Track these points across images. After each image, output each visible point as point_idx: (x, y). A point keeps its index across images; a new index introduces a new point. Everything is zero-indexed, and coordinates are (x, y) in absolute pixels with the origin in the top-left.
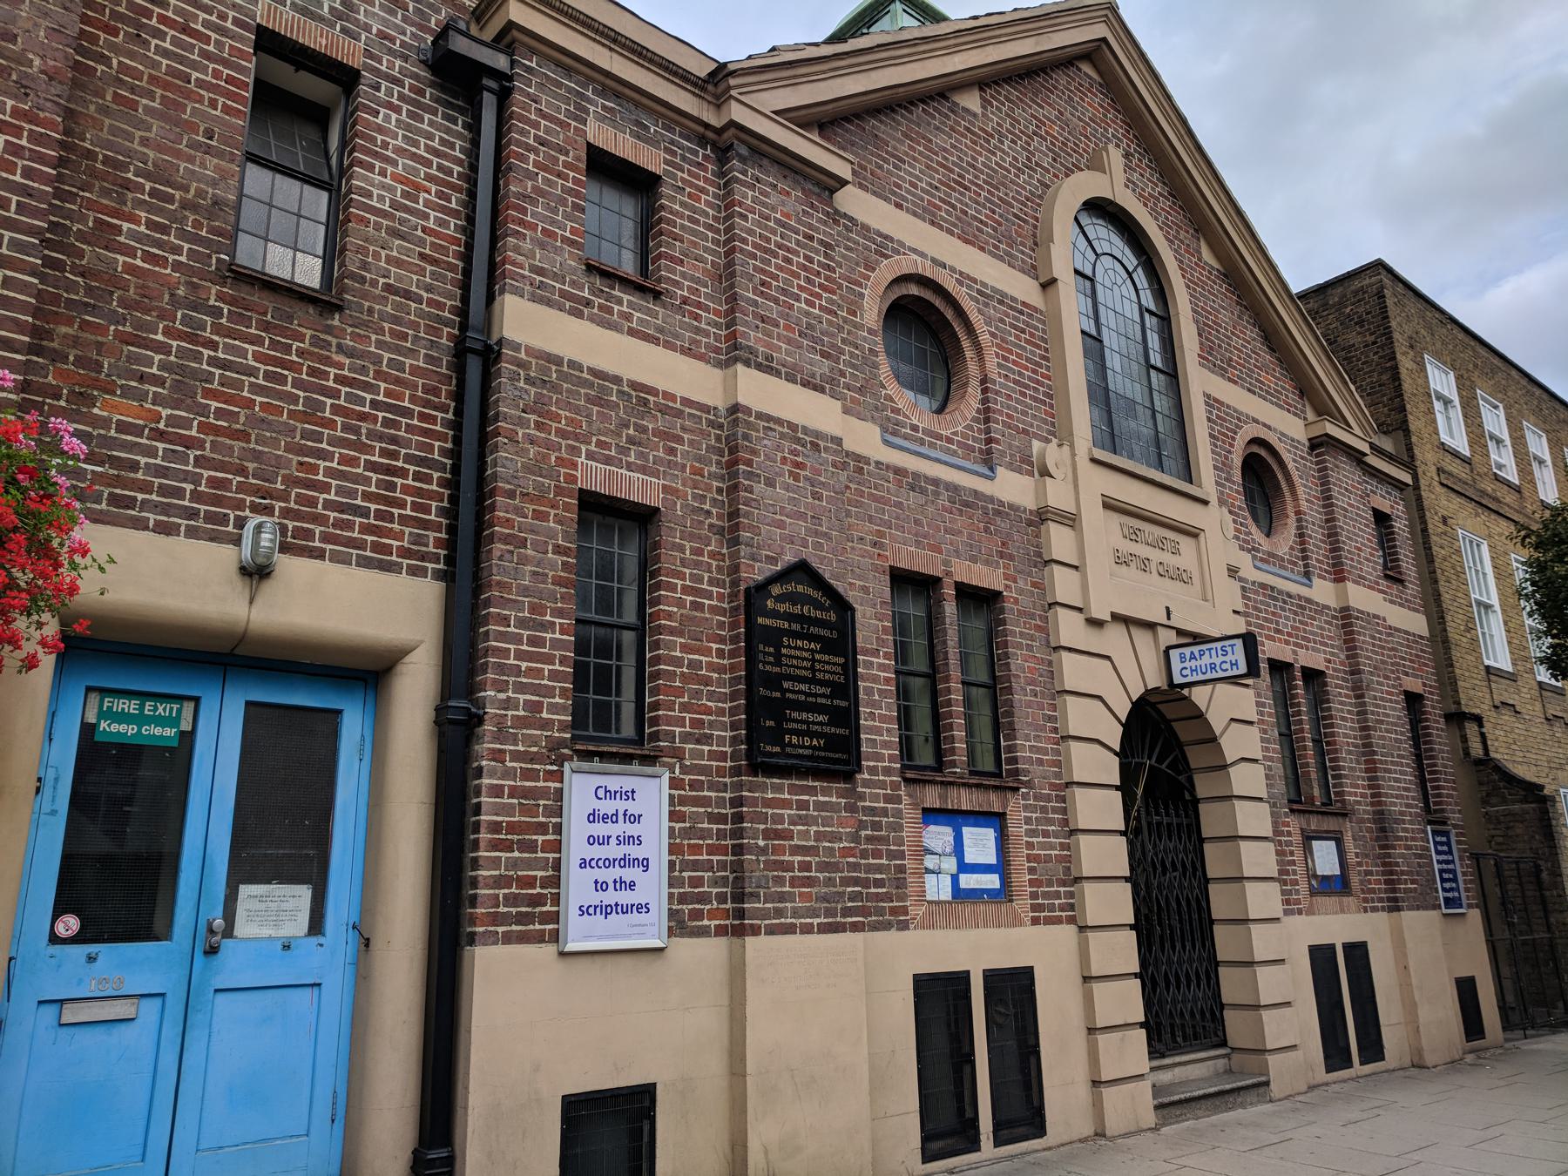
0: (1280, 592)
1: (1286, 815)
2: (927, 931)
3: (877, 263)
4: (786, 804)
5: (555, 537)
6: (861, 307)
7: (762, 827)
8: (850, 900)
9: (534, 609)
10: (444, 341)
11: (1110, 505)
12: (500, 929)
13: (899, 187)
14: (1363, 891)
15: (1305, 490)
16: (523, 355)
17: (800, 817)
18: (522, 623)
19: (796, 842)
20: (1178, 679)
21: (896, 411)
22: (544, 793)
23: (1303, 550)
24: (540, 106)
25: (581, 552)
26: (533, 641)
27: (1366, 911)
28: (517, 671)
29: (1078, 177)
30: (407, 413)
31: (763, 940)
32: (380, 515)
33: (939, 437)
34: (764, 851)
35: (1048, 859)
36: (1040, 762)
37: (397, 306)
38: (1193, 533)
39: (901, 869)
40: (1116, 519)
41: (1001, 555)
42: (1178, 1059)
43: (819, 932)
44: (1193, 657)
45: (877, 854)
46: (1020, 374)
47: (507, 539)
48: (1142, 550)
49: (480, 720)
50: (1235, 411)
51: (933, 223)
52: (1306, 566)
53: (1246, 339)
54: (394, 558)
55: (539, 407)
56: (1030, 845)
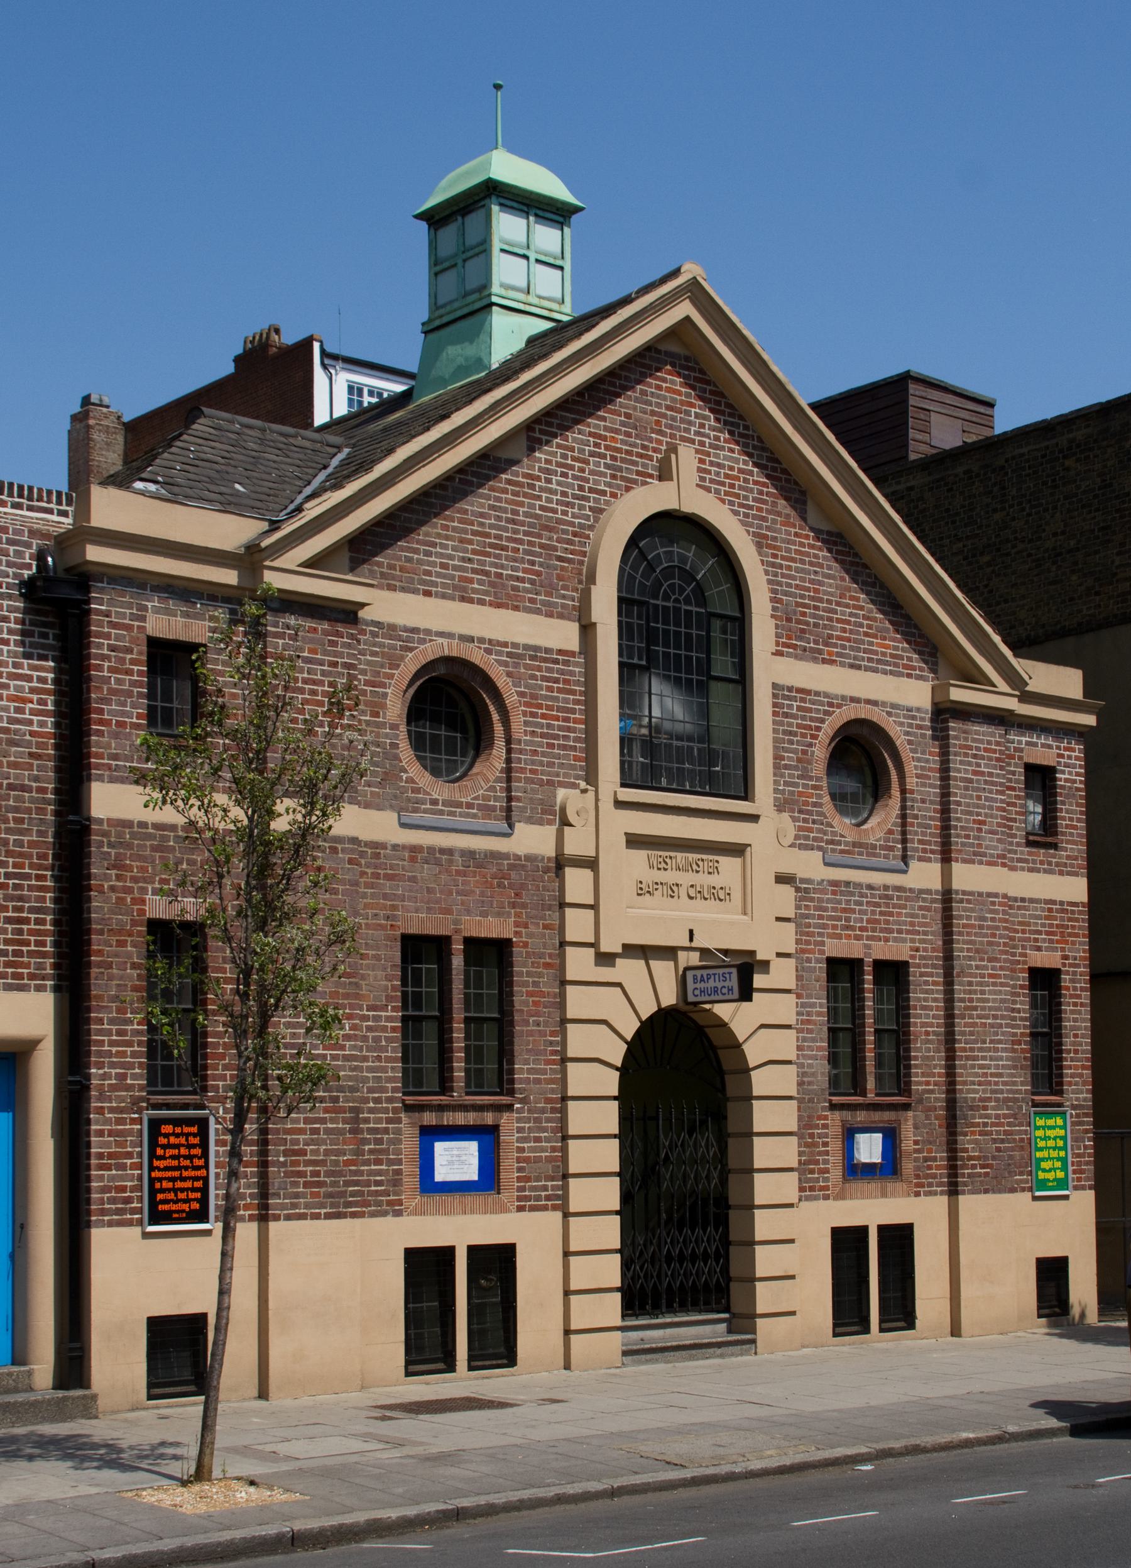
0: (859, 885)
1: (823, 1109)
2: (419, 1217)
3: (402, 658)
4: (301, 1131)
5: (131, 957)
6: (383, 706)
7: (282, 1148)
8: (351, 1196)
9: (119, 1011)
10: (49, 817)
11: (635, 841)
12: (106, 1218)
13: (429, 573)
14: (918, 1177)
15: (917, 762)
16: (105, 827)
17: (312, 1140)
18: (112, 1021)
19: (308, 1157)
20: (691, 998)
21: (417, 790)
22: (130, 1132)
23: (904, 833)
24: (107, 610)
25: (151, 973)
26: (120, 1033)
27: (917, 1194)
28: (110, 1054)
29: (638, 492)
30: (27, 877)
31: (282, 1224)
32: (16, 953)
33: (459, 805)
34: (284, 1164)
35: (538, 1160)
36: (538, 1081)
37: (17, 799)
38: (737, 850)
39: (398, 1172)
40: (641, 855)
41: (513, 905)
42: (668, 1320)
43: (325, 1218)
44: (702, 980)
45: (378, 1162)
46: (549, 726)
47: (99, 965)
48: (670, 877)
49: (87, 1088)
50: (826, 695)
51: (463, 599)
52: (905, 849)
53: (859, 609)
54: (26, 981)
55: (118, 865)
56: (521, 1150)
